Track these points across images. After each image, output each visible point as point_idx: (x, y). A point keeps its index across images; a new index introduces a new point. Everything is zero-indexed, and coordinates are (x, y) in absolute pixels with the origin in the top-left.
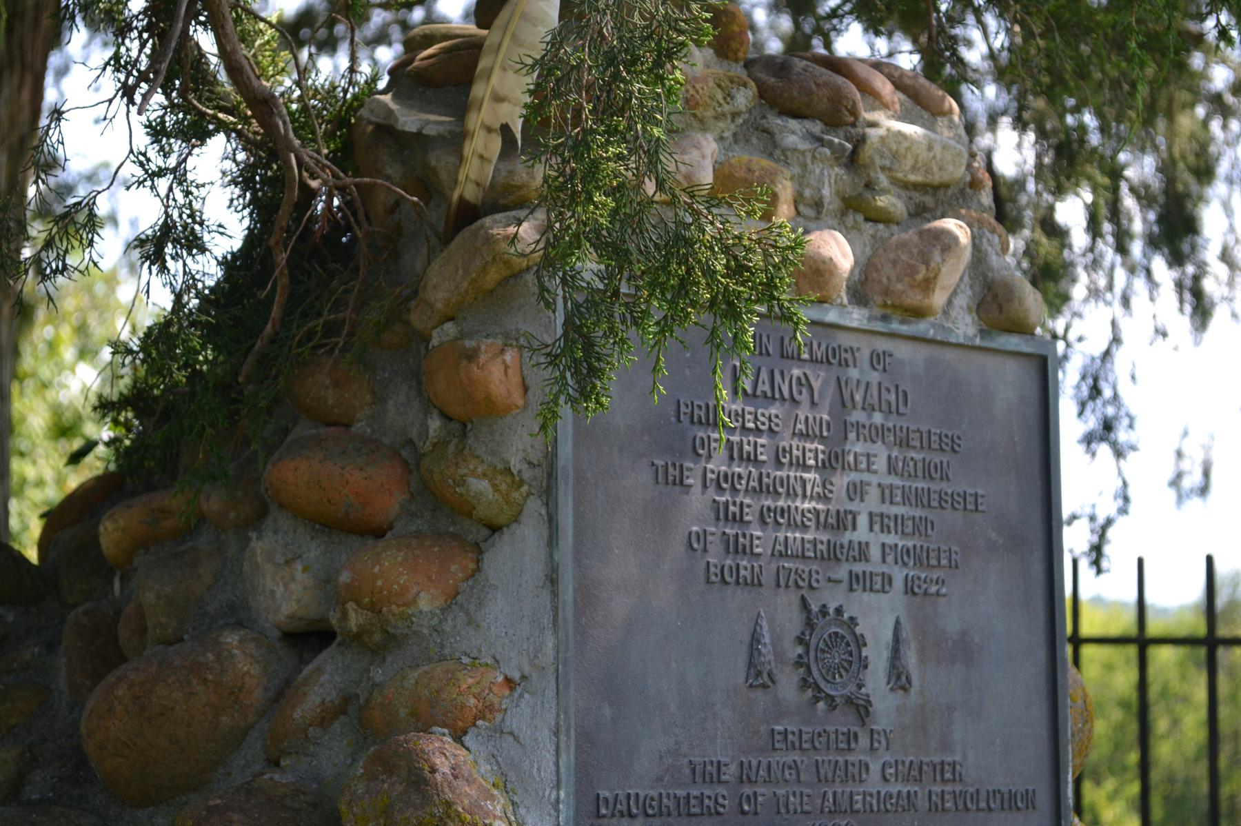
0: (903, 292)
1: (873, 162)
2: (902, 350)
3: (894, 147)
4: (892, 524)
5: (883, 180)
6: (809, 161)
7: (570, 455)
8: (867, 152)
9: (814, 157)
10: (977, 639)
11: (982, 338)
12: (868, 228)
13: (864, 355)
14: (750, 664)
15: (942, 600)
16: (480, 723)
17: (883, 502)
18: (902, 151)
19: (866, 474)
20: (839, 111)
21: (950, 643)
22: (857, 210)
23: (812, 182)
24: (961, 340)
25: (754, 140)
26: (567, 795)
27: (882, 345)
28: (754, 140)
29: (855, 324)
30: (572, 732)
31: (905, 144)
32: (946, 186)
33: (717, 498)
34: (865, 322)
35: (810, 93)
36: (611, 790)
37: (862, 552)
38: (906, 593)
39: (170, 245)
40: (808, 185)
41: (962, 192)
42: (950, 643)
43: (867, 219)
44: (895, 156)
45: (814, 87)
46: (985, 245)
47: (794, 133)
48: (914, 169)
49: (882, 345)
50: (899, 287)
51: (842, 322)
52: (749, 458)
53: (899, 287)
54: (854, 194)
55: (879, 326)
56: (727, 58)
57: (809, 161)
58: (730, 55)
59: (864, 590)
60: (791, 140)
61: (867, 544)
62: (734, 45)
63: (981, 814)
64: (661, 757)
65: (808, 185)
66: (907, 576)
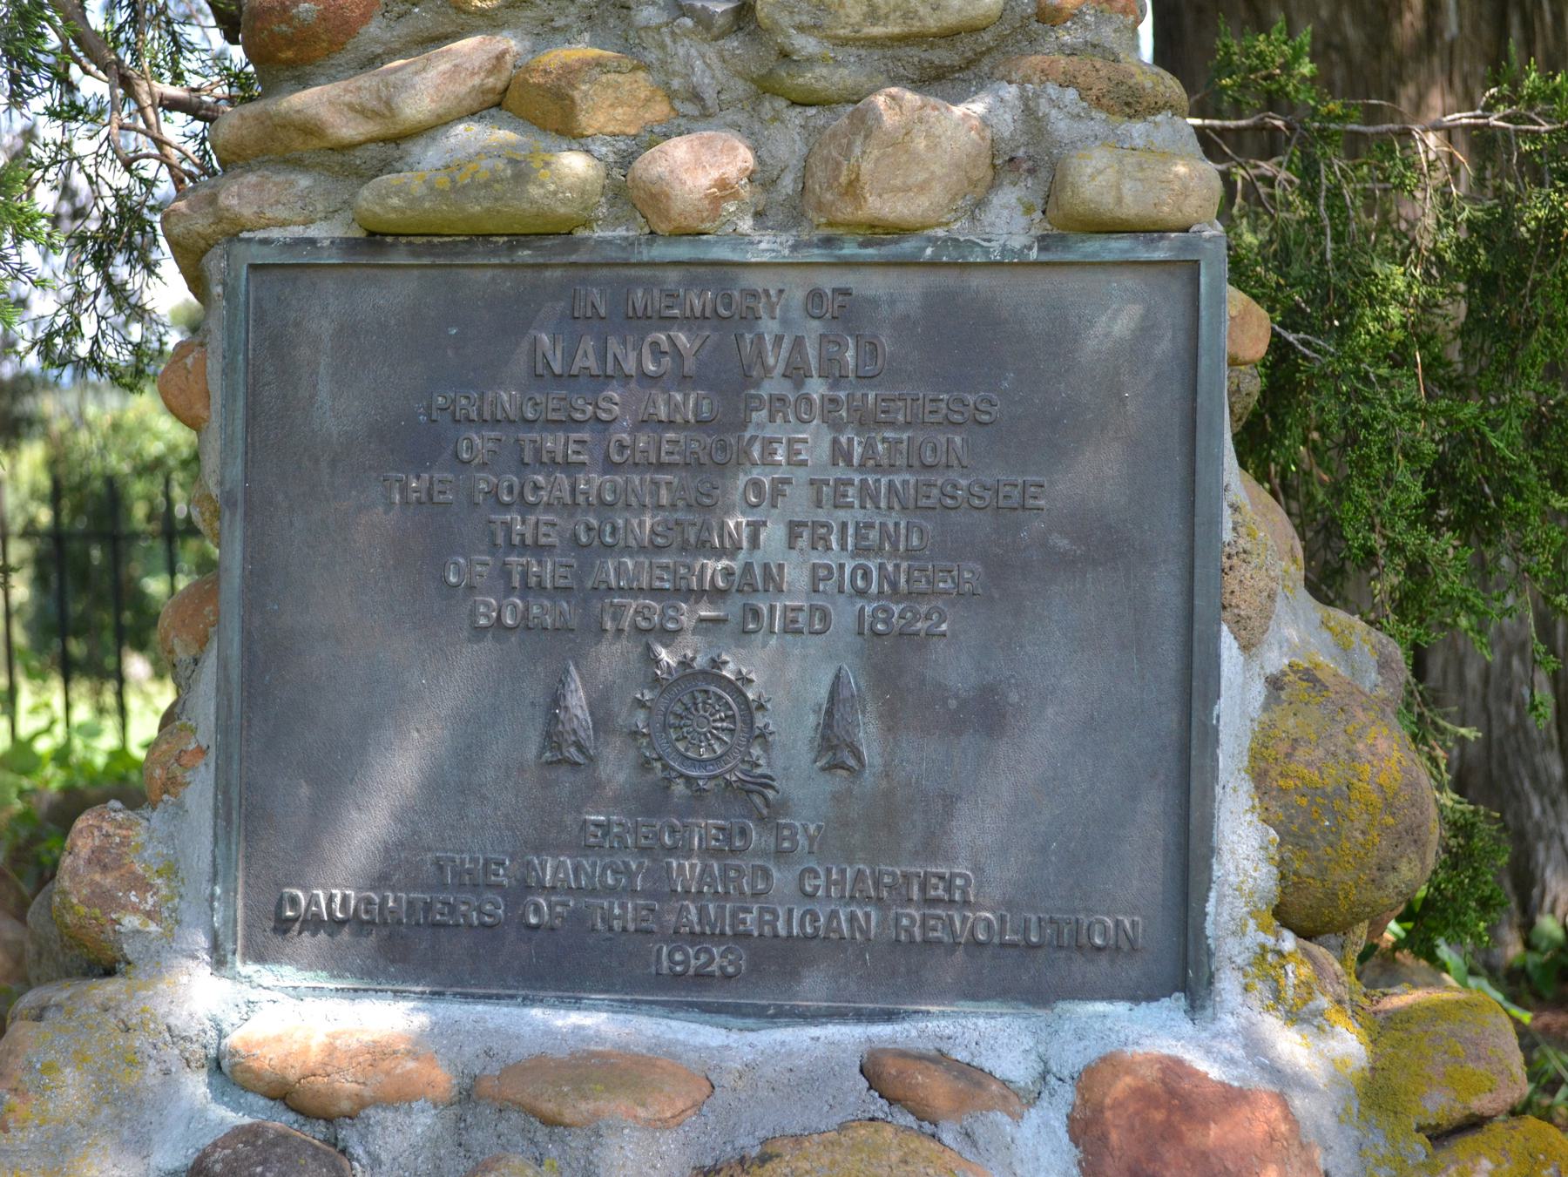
0: (833, 203)
2: (873, 284)
6: (668, 40)
7: (343, 84)
13: (798, 295)
14: (548, 735)
17: (819, 505)
19: (1020, 512)
21: (953, 704)
22: (775, 94)
23: (678, 68)
30: (235, 815)
33: (493, 517)
39: (170, 347)
40: (674, 73)
42: (953, 704)
43: (794, 103)
46: (1043, 107)
49: (828, 281)
50: (829, 196)
53: (829, 196)
54: (764, 72)
57: (668, 40)
65: (674, 73)
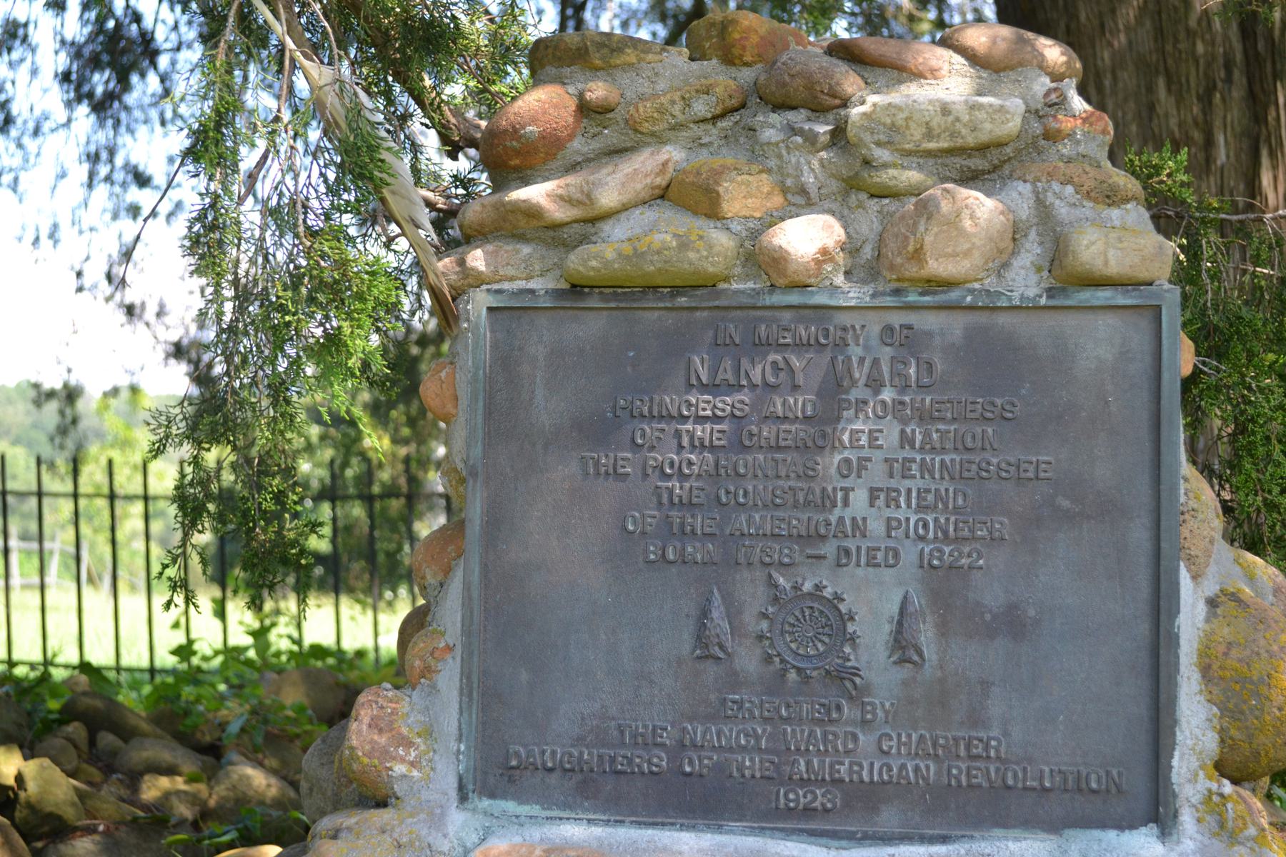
0: (902, 265)
1: (861, 140)
3: (888, 121)
4: (902, 500)
5: (882, 155)
6: (784, 152)
8: (851, 132)
9: (787, 147)
10: (1032, 613)
11: (1049, 297)
12: (873, 205)
13: (876, 329)
14: (699, 638)
15: (977, 575)
16: (423, 680)
17: (891, 476)
18: (900, 122)
20: (816, 97)
21: (988, 617)
22: (859, 189)
24: (1017, 302)
25: (742, 140)
26: (468, 748)
27: (897, 319)
28: (742, 140)
29: (853, 303)
30: (475, 694)
31: (902, 116)
32: (1000, 145)
34: (868, 299)
35: (784, 85)
36: (525, 746)
37: (859, 527)
38: (922, 567)
40: (788, 175)
41: (1034, 143)
43: (872, 196)
44: (893, 128)
45: (787, 78)
46: (1050, 198)
47: (773, 127)
48: (929, 134)
49: (897, 319)
50: (899, 260)
51: (833, 303)
52: (702, 445)
55: (889, 301)
56: (734, 64)
57: (784, 152)
58: (737, 61)
59: (858, 565)
60: (769, 135)
61: (864, 519)
62: (736, 51)
63: (1067, 796)
64: (583, 719)
66: (923, 550)
